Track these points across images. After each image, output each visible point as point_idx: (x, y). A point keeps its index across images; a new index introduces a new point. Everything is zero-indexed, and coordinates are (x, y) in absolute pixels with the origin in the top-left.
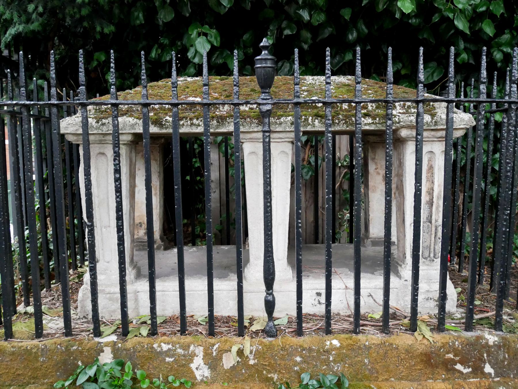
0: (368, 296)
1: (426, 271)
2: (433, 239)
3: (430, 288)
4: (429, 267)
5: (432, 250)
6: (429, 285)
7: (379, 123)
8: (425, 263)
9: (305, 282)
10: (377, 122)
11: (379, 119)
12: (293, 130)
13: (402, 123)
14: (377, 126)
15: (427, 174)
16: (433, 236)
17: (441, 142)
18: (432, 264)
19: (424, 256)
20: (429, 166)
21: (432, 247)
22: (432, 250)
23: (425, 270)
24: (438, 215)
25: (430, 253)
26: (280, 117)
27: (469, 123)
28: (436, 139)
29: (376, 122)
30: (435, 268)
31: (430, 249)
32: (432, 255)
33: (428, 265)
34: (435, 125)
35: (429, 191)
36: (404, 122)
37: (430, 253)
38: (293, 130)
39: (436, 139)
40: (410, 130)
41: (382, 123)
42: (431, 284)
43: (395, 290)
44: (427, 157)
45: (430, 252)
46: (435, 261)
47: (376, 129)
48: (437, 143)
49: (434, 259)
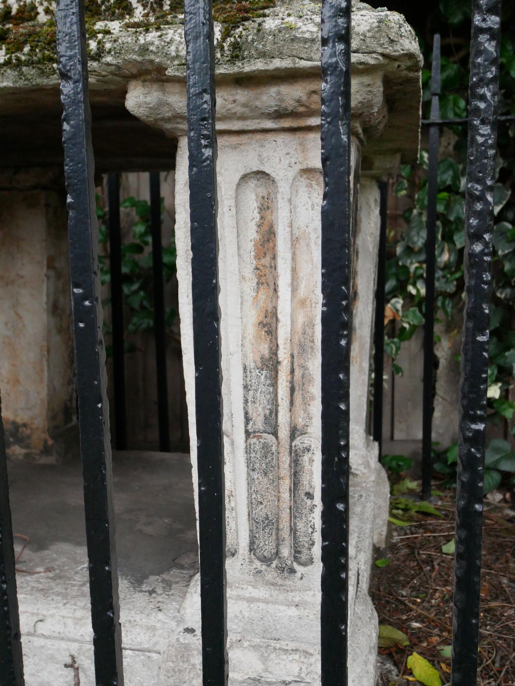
0: (66, 666)
1: (262, 605)
2: (286, 495)
3: (266, 670)
4: (275, 593)
5: (285, 533)
6: (265, 660)
7: (29, 63)
8: (263, 577)
9: (23, 579)
10: (23, 58)
11: (32, 50)
12: (145, 176)
13: (109, 59)
14: (21, 74)
15: (257, 257)
16: (286, 484)
17: (299, 135)
18: (288, 582)
19: (259, 553)
20: (266, 228)
21: (285, 524)
22: (285, 533)
23: (258, 600)
24: (305, 411)
25: (278, 545)
26: (407, 215)
27: (373, 45)
28: (269, 124)
29: (18, 59)
30: (297, 599)
31: (278, 529)
32: (286, 552)
33: (274, 584)
34: (234, 58)
35: (268, 320)
36: (118, 54)
37: (278, 545)
38: (145, 176)
39: (269, 124)
40: (155, 86)
41: (39, 62)
42: (273, 656)
43: (154, 656)
44: (253, 197)
45: (277, 539)
46: (298, 575)
47: (21, 83)
48: (282, 138)
49: (296, 566)
